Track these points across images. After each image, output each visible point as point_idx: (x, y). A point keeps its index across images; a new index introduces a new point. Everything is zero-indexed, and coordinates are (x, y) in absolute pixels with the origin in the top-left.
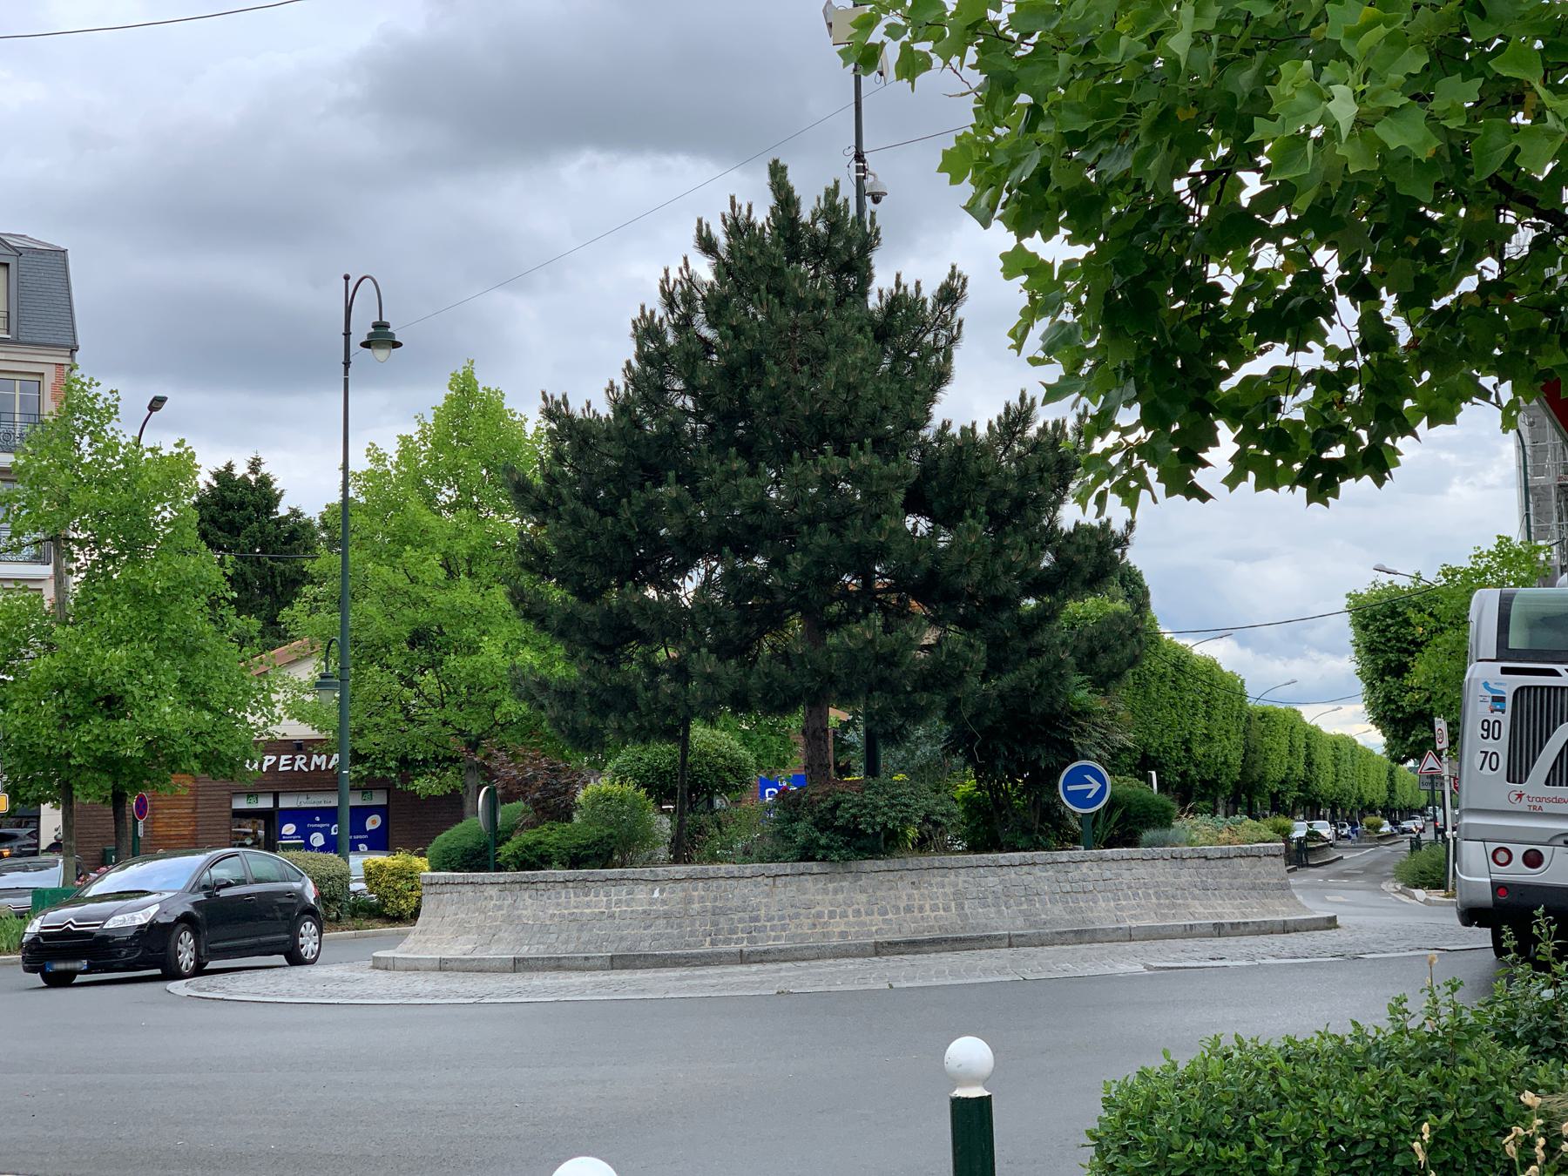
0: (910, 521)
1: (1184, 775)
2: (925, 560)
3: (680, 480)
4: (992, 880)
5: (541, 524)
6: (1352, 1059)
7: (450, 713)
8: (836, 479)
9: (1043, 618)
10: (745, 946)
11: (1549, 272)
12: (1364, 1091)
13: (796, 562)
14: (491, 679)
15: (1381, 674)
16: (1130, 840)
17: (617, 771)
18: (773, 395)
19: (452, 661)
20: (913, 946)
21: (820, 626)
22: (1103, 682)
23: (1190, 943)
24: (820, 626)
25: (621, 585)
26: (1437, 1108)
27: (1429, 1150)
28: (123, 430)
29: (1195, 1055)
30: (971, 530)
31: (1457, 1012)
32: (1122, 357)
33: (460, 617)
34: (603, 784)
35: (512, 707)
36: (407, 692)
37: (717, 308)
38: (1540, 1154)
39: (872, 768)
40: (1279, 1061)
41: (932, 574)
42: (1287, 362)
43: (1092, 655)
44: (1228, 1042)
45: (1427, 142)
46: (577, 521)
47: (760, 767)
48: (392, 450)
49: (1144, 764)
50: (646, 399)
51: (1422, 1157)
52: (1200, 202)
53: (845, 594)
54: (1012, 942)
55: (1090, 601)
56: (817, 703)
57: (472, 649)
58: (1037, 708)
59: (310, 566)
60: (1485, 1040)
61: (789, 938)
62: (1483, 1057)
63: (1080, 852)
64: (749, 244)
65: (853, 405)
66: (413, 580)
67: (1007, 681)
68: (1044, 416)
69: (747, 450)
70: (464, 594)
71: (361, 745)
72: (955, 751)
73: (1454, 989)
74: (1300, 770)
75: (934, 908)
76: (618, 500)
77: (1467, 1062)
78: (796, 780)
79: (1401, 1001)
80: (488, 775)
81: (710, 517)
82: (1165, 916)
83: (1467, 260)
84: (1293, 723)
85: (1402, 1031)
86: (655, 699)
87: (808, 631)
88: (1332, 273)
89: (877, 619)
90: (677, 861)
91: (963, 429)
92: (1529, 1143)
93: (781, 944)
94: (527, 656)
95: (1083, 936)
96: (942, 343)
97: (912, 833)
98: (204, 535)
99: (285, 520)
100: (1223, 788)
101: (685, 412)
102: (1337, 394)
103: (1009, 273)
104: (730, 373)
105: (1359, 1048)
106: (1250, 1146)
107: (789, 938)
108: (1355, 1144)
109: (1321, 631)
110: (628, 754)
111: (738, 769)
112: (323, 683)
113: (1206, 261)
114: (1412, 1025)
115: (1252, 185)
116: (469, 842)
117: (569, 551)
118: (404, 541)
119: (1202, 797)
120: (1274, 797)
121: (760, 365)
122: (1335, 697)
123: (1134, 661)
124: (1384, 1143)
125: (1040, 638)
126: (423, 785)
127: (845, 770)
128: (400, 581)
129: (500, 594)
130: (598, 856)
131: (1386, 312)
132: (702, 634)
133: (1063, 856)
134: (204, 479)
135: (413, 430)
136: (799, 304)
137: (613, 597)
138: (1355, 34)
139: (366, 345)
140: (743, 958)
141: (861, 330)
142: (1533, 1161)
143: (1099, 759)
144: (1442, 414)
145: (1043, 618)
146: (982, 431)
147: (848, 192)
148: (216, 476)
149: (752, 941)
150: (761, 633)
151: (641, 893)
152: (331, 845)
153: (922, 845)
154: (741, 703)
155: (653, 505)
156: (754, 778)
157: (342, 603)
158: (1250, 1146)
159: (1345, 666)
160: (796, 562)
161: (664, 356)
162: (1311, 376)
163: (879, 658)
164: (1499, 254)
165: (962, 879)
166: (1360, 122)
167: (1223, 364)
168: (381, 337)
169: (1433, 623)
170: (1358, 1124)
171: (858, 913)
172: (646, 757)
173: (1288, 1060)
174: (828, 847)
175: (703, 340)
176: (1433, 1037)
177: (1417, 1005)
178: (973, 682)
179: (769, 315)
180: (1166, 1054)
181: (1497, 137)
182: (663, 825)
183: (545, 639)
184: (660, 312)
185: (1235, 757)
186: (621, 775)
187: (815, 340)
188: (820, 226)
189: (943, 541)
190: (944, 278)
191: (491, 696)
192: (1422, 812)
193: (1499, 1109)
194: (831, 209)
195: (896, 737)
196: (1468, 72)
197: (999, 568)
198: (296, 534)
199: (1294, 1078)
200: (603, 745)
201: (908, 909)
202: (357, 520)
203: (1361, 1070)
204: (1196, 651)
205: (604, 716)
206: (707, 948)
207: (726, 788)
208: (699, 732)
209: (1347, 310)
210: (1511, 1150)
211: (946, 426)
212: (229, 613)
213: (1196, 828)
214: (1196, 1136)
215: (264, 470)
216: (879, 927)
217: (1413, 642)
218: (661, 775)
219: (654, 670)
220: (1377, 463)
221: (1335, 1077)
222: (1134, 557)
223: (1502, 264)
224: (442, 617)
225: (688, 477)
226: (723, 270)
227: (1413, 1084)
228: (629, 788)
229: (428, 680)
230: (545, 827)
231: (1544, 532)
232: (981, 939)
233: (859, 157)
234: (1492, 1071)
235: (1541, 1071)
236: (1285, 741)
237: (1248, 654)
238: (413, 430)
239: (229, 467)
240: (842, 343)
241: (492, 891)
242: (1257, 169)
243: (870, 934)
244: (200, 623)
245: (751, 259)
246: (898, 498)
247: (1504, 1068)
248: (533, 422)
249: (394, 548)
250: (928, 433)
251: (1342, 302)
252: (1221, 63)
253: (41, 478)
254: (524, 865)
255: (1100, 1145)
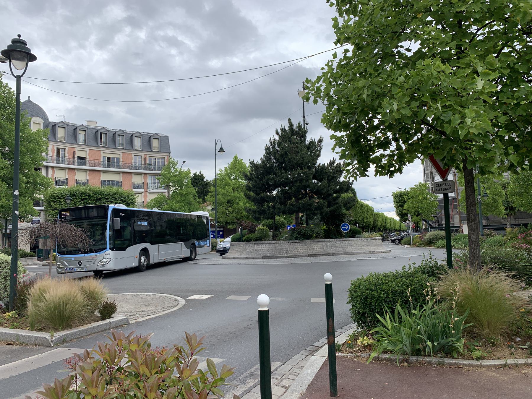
0: (313, 181)
1: (363, 225)
2: (316, 188)
3: (273, 174)
4: (329, 244)
5: (249, 182)
6: (396, 277)
7: (234, 215)
8: (301, 174)
9: (337, 197)
10: (285, 255)
11: (430, 136)
12: (398, 282)
13: (294, 188)
14: (241, 209)
15: (399, 207)
16: (353, 237)
17: (263, 224)
18: (289, 159)
19: (234, 206)
20: (315, 255)
21: (298, 199)
22: (348, 209)
23: (365, 255)
24: (298, 199)
25: (263, 193)
26: (411, 285)
27: (410, 293)
28: (178, 167)
29: (368, 275)
30: (324, 182)
31: (415, 268)
32: (354, 152)
33: (236, 198)
34: (260, 227)
35: (245, 213)
36: (227, 211)
37: (279, 144)
38: (430, 294)
39: (307, 224)
40: (382, 277)
41: (317, 190)
42: (383, 153)
43: (346, 204)
44: (373, 274)
45: (410, 113)
46: (256, 181)
47: (288, 224)
48: (223, 169)
49: (355, 224)
50: (267, 160)
51: (409, 294)
52: (367, 125)
53: (302, 193)
54: (333, 255)
55: (345, 194)
56: (297, 213)
57: (238, 204)
58: (337, 213)
59: (210, 190)
60: (420, 273)
61: (293, 254)
62: (420, 276)
63: (345, 239)
64: (285, 133)
65: (303, 161)
66: (228, 192)
67: (331, 209)
68: (338, 161)
69: (285, 169)
70: (236, 194)
71: (219, 220)
72: (322, 221)
73: (414, 264)
74: (384, 224)
75: (319, 249)
76: (263, 178)
77: (416, 277)
78: (294, 226)
79: (404, 266)
80: (241, 225)
81: (279, 181)
82: (360, 250)
83: (415, 134)
84: (382, 215)
85: (404, 272)
86: (269, 212)
87: (296, 200)
88: (391, 137)
89: (308, 198)
90: (273, 240)
91: (323, 165)
92: (428, 292)
93: (292, 255)
94: (247, 205)
95: (345, 254)
96: (319, 149)
97: (314, 235)
98: (192, 184)
99: (205, 181)
100: (370, 227)
101: (274, 162)
102: (392, 158)
103: (331, 139)
104: (282, 155)
105: (397, 275)
106: (377, 292)
107: (293, 254)
108: (396, 291)
109: (387, 199)
110: (265, 221)
111: (284, 224)
112: (212, 210)
113: (368, 135)
114: (406, 270)
115: (376, 122)
116: (238, 237)
117: (254, 187)
118: (226, 185)
119: (366, 229)
120: (379, 229)
121: (287, 154)
122: (390, 211)
123: (354, 205)
124: (402, 291)
125: (337, 201)
126: (230, 227)
127: (302, 224)
128: (225, 192)
129: (242, 194)
130: (260, 239)
131: (401, 143)
132: (277, 201)
133: (342, 239)
134: (192, 175)
135: (227, 166)
136: (294, 143)
137: (262, 195)
138: (397, 94)
139: (219, 151)
140: (285, 257)
141: (304, 147)
142: (429, 295)
143: (348, 222)
144: (411, 161)
145: (337, 197)
146: (326, 165)
147: (302, 123)
148: (194, 174)
149: (287, 254)
150: (287, 201)
151: (267, 246)
152: (214, 237)
153: (316, 237)
154: (284, 213)
155: (269, 179)
156: (287, 225)
157: (216, 195)
158: (377, 292)
159: (391, 205)
160: (294, 188)
161: (270, 153)
162: (387, 155)
163: (308, 205)
164: (421, 133)
165: (323, 243)
166: (397, 110)
167: (371, 154)
168: (222, 150)
169: (408, 198)
170: (397, 288)
171: (305, 249)
172: (268, 222)
173: (384, 277)
174: (300, 238)
175: (277, 150)
176: (410, 273)
177: (407, 267)
178: (325, 209)
179: (288, 145)
180: (362, 276)
181: (422, 112)
182: (271, 234)
183: (250, 202)
184: (269, 145)
185: (372, 222)
186: (263, 225)
187: (296, 149)
188: (297, 129)
189: (319, 184)
190: (319, 138)
191: (241, 212)
192: (406, 231)
193: (422, 286)
194: (299, 126)
195: (311, 219)
196: (417, 100)
197: (329, 189)
198: (207, 184)
199: (385, 280)
200: (260, 220)
201: (314, 249)
202: (218, 181)
203: (397, 279)
204: (365, 203)
205: (261, 215)
206: (279, 255)
207: (282, 227)
208: (277, 218)
209: (394, 144)
210: (425, 293)
211: (320, 164)
212: (197, 198)
213: (365, 234)
214: (368, 290)
215: (202, 173)
216: (309, 252)
217: (404, 201)
218: (270, 225)
219: (269, 207)
220: (400, 170)
221: (393, 280)
222: (354, 186)
223: (422, 134)
224: (233, 198)
225: (275, 174)
226: (280, 138)
227: (407, 281)
228: (265, 227)
229: (230, 209)
230: (250, 234)
231: (428, 181)
232: (327, 254)
233: (304, 117)
234: (421, 279)
235: (430, 279)
236: (381, 219)
237: (374, 203)
238: (227, 166)
239: (196, 173)
240: (301, 150)
241: (242, 245)
242: (377, 119)
243: (307, 253)
244: (192, 199)
245: (285, 136)
246: (311, 177)
247: (423, 278)
248: (248, 165)
249: (224, 186)
250: (317, 165)
251: (393, 142)
252: (372, 100)
253: (165, 175)
254: (247, 241)
255: (350, 292)
